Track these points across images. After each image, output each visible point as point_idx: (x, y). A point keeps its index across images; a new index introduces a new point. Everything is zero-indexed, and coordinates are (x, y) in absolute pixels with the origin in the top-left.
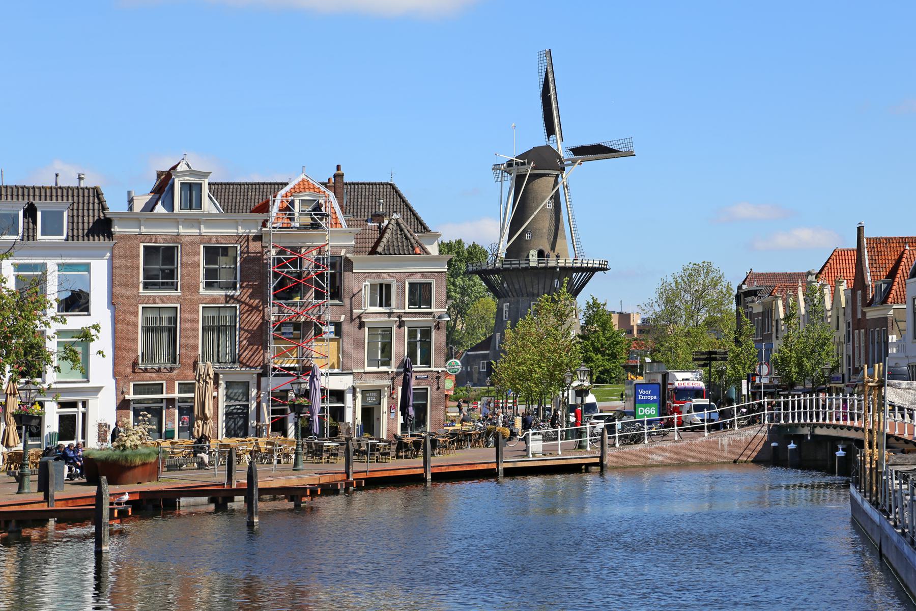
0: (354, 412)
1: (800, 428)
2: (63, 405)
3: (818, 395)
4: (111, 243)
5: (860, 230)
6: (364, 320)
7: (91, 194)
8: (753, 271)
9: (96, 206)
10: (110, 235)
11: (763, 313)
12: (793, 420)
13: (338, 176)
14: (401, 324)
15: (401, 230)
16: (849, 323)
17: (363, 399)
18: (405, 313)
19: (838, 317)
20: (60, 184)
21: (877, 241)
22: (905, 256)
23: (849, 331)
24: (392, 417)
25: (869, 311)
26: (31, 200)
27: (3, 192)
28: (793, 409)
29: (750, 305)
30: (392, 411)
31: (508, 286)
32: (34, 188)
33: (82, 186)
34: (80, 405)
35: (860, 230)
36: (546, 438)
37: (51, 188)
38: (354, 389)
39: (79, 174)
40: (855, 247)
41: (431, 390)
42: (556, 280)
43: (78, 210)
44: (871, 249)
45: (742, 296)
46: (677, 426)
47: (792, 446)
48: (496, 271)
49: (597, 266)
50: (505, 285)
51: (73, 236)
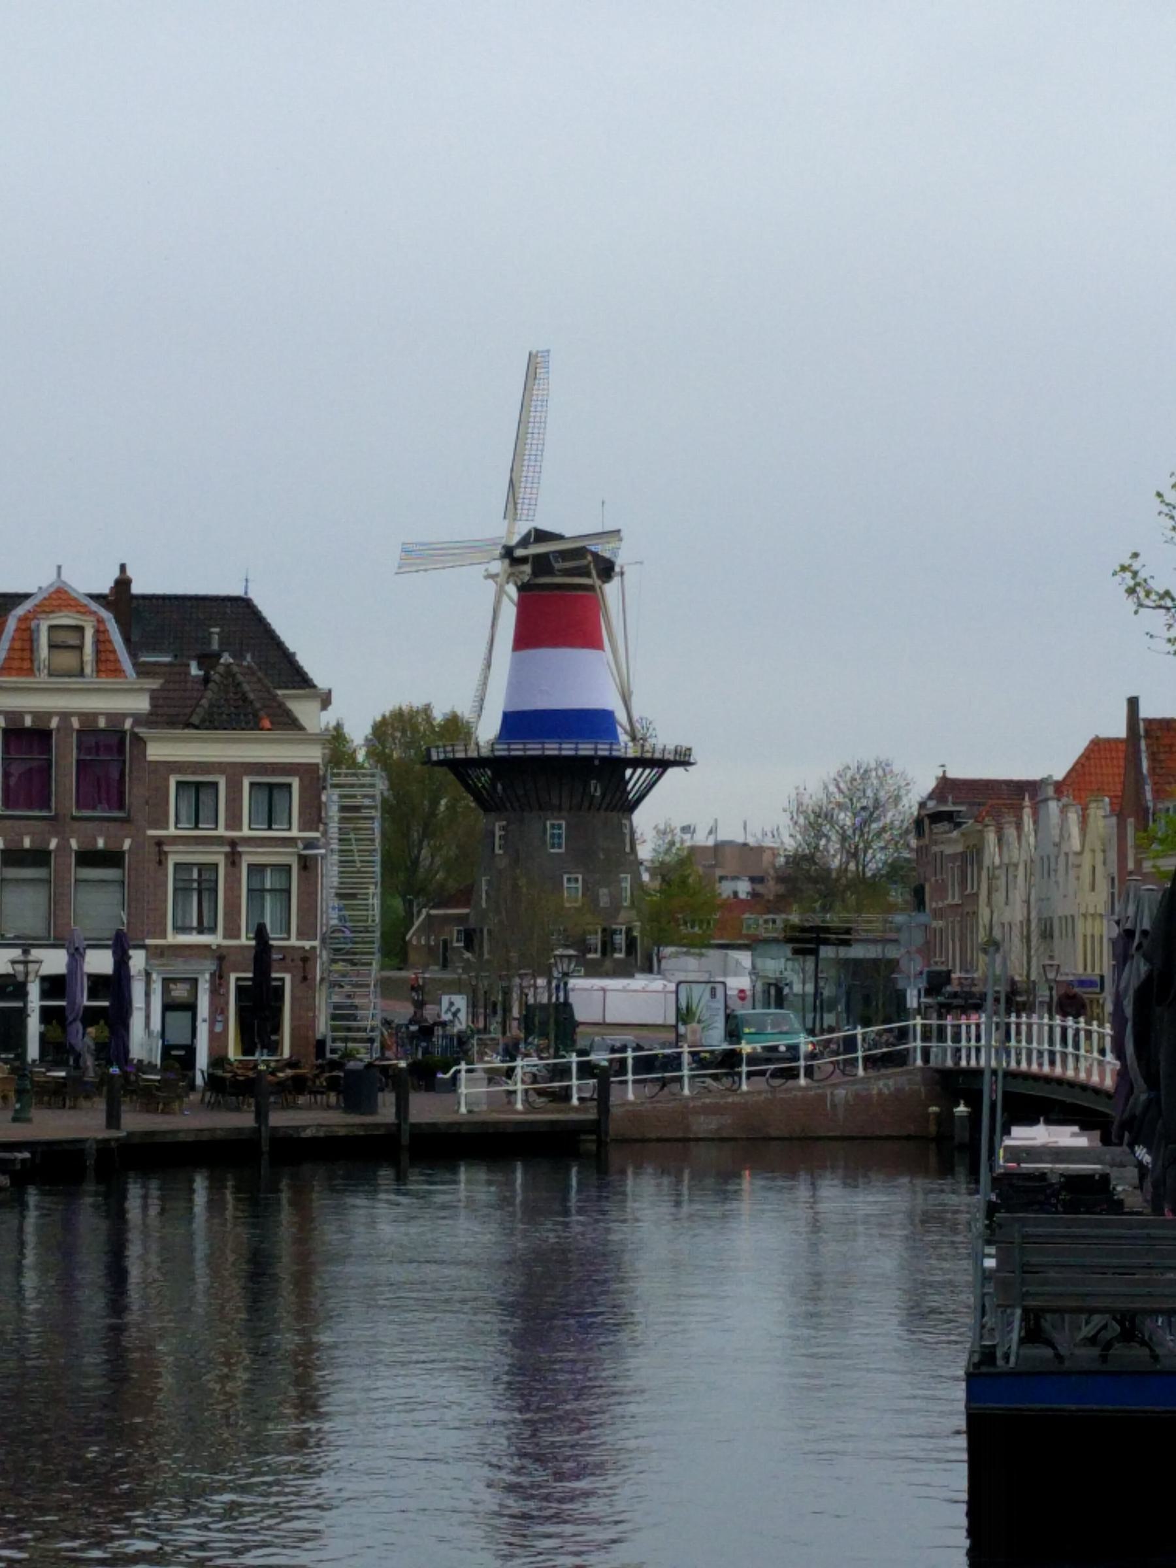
0: (148, 1017)
3: (1018, 1016)
5: (1133, 703)
6: (240, 849)
8: (952, 774)
12: (968, 1061)
13: (123, 583)
14: (233, 859)
16: (1113, 879)
17: (166, 991)
19: (1094, 868)
23: (1113, 894)
24: (218, 1028)
28: (969, 1040)
30: (219, 1018)
31: (504, 789)
36: (492, 1076)
42: (593, 782)
45: (927, 821)
46: (634, 1073)
48: (481, 762)
49: (671, 757)
50: (499, 787)
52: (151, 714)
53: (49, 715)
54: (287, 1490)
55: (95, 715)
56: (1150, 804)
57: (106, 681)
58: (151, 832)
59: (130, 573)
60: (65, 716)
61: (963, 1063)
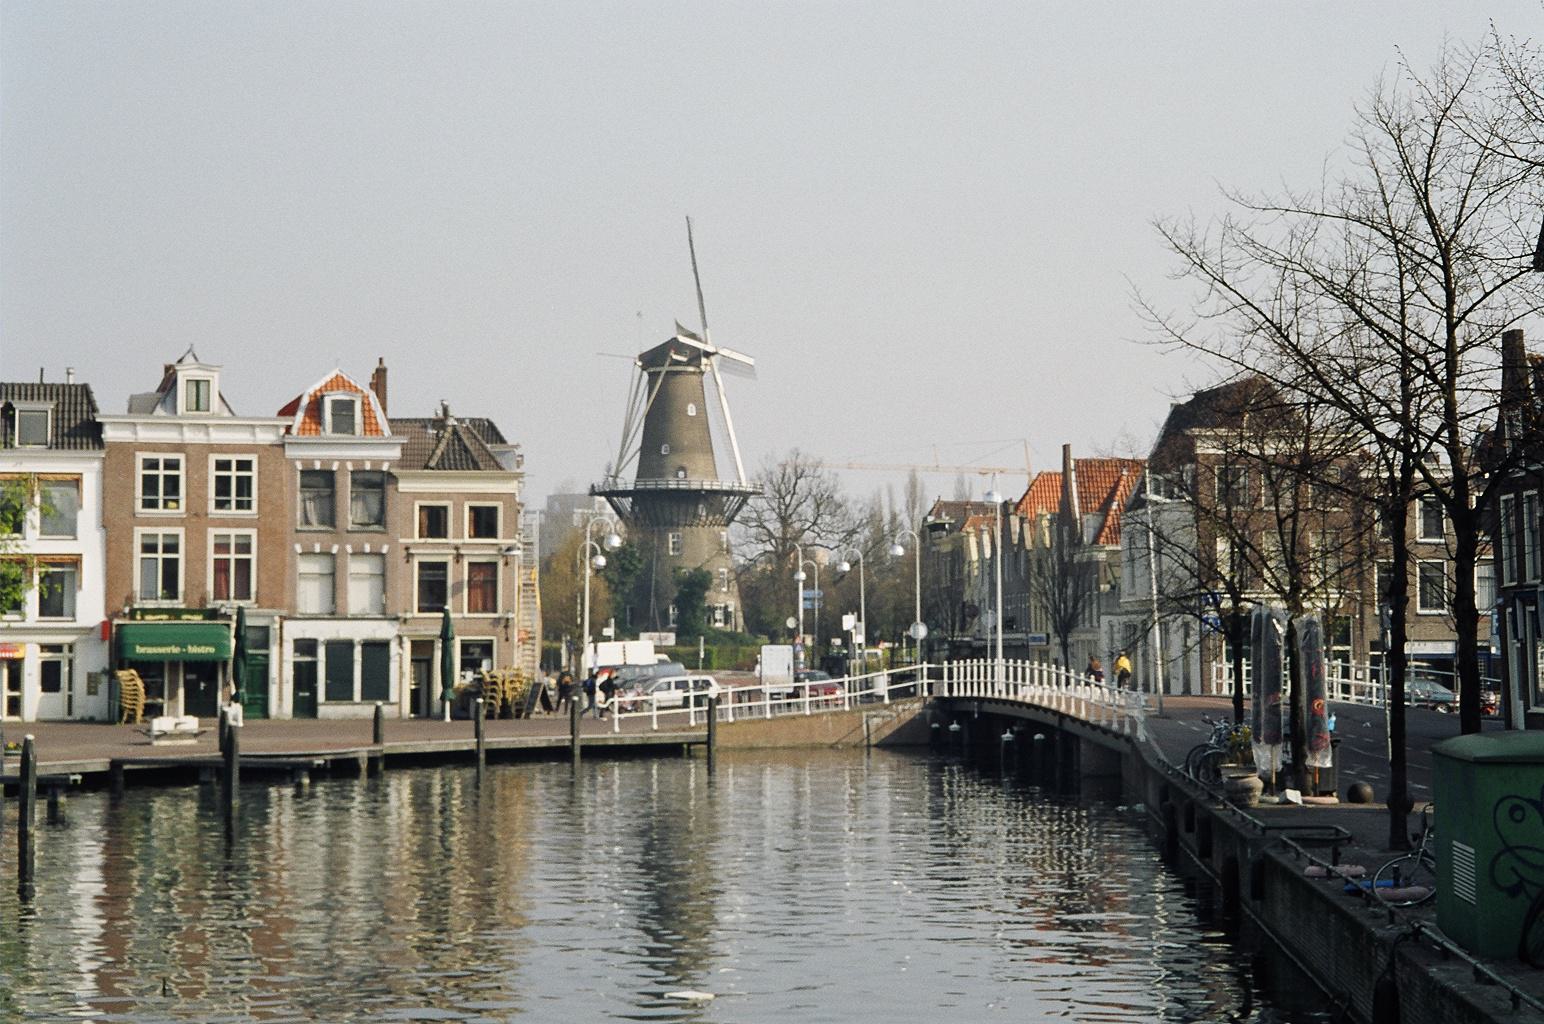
1: (986, 704)
2: (44, 647)
4: (103, 455)
5: (1066, 448)
7: (79, 392)
8: (943, 499)
9: (85, 408)
10: (99, 443)
11: (953, 551)
14: (458, 557)
15: (460, 439)
18: (464, 544)
20: (45, 381)
21: (1088, 463)
22: (1122, 483)
25: (270, 419)
26: (10, 400)
27: (4, 391)
29: (937, 541)
32: (13, 385)
33: (71, 382)
34: (66, 649)
35: (1066, 448)
37: (33, 385)
38: (400, 638)
39: (68, 369)
40: (1060, 470)
41: (498, 641)
43: (63, 411)
44: (1080, 474)
45: (928, 531)
47: (954, 726)
51: (57, 444)
52: (401, 460)
53: (331, 461)
54: (1038, 612)
55: (362, 461)
56: (1078, 516)
57: (370, 439)
58: (402, 541)
59: (386, 364)
60: (343, 462)
61: (955, 694)
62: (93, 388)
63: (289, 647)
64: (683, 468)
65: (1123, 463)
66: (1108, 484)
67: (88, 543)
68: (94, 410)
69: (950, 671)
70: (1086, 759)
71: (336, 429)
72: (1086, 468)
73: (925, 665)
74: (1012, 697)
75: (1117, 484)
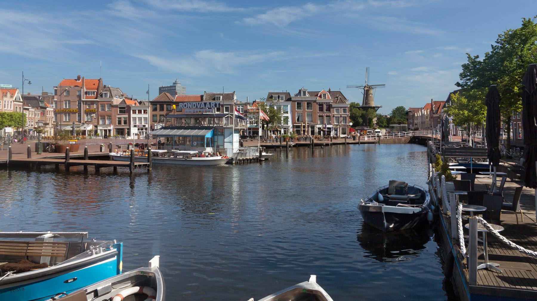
5: (432, 99)
21: (435, 102)
35: (432, 99)
47: (417, 140)
61: (424, 136)
62: (290, 93)
63: (317, 129)
64: (369, 104)
65: (441, 102)
66: (439, 105)
67: (289, 115)
68: (290, 96)
69: (416, 132)
70: (111, 157)
71: (124, 124)
72: (435, 102)
73: (388, 134)
74: (427, 136)
75: (440, 105)
